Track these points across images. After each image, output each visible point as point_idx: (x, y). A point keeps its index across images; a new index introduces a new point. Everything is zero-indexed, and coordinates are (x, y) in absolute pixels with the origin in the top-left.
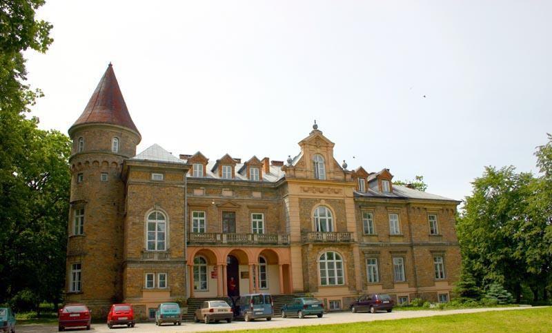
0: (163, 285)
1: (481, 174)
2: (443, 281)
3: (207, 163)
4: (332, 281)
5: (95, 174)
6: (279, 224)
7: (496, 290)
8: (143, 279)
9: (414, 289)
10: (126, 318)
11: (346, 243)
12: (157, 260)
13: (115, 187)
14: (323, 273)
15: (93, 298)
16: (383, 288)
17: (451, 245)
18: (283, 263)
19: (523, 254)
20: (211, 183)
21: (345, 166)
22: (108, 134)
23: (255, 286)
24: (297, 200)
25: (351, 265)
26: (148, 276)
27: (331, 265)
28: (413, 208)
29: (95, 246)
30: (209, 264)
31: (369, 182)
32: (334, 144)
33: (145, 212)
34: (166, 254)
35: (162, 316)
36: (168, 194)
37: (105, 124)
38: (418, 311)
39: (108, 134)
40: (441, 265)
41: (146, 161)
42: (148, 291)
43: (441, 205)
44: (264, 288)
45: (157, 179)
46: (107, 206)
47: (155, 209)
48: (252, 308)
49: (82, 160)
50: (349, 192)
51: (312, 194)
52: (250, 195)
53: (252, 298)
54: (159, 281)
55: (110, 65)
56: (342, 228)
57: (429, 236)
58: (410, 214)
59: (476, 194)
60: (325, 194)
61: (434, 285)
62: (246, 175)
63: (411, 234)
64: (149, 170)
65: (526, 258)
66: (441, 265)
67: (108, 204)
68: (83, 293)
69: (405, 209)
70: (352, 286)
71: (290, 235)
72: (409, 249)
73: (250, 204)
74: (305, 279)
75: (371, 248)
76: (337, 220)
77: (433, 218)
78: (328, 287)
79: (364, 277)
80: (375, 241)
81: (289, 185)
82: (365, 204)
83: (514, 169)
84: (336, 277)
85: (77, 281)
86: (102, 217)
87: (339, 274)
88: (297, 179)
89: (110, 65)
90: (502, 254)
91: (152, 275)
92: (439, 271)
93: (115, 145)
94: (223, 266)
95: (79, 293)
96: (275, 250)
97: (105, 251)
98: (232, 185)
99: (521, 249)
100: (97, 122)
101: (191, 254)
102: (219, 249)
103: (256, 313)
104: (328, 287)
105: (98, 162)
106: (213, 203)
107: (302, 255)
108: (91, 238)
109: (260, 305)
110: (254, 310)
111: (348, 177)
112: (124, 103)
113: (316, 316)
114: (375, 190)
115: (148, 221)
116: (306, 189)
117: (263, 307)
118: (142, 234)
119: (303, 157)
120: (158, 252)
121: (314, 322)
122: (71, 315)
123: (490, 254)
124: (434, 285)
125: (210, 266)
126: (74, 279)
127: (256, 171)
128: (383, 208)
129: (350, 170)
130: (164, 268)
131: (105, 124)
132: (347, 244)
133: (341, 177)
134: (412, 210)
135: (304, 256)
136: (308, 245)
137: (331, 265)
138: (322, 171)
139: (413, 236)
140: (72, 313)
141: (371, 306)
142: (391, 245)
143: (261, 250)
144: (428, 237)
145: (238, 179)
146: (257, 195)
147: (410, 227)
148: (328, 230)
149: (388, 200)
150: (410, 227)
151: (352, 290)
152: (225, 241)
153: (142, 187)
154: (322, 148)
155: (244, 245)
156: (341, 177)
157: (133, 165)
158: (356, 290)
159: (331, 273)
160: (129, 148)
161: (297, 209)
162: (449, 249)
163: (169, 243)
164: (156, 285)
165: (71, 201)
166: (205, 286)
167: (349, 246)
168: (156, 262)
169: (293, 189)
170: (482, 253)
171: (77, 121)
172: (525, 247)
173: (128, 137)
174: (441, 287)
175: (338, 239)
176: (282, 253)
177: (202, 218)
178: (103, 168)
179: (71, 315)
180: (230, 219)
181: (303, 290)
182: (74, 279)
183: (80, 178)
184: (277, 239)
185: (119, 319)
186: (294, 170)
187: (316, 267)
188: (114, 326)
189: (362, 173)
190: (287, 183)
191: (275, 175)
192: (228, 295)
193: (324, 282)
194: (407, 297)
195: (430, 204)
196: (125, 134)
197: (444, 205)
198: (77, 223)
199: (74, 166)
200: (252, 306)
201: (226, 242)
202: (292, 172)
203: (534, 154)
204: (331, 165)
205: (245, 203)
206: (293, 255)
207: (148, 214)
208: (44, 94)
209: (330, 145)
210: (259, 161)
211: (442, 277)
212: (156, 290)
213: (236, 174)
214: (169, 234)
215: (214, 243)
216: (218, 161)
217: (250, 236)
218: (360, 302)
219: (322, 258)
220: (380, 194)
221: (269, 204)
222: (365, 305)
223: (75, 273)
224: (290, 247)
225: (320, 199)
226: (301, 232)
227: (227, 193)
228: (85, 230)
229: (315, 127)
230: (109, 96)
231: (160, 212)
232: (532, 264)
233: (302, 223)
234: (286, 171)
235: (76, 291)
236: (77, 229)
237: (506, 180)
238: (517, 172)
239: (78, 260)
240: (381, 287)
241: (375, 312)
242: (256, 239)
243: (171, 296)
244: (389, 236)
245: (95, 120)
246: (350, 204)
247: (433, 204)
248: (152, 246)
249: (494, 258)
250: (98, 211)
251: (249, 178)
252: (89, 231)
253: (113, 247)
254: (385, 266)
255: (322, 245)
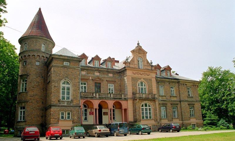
0: (69, 117)
1: (206, 70)
2: (193, 118)
3: (87, 59)
4: (147, 117)
5: (33, 61)
6: (121, 89)
7: (222, 122)
8: (59, 115)
9: (181, 122)
10: (58, 135)
11: (153, 99)
12: (66, 105)
13: (43, 68)
14: (143, 113)
15: (31, 124)
16: (168, 121)
17: (197, 101)
18: (124, 108)
19: (226, 107)
20: (90, 68)
21: (152, 63)
22: (40, 42)
23: (111, 119)
24: (131, 78)
25: (155, 110)
26: (62, 113)
27: (146, 110)
28: (181, 84)
29: (32, 98)
30: (88, 108)
31: (161, 71)
32: (147, 52)
33: (61, 81)
34: (71, 102)
35: (76, 134)
36: (72, 72)
37: (38, 37)
38: (193, 132)
39: (40, 42)
40: (192, 110)
41: (61, 55)
42: (62, 121)
43: (193, 83)
44: (86, 121)
45: (66, 65)
46: (39, 78)
47: (65, 80)
48: (119, 130)
49: (27, 54)
50: (154, 75)
51: (137, 76)
52: (108, 75)
53: (118, 124)
54: (67, 116)
55: (40, 9)
56: (151, 92)
57: (188, 97)
58: (180, 87)
59: (203, 79)
60: (143, 76)
61: (190, 120)
62: (105, 66)
63: (180, 96)
64: (62, 60)
65: (228, 108)
66: (192, 110)
67: (39, 77)
68: (26, 122)
69: (177, 84)
70: (156, 120)
71: (127, 95)
72: (179, 103)
73: (107, 79)
74: (135, 116)
75: (163, 102)
76: (148, 88)
77: (189, 89)
78: (145, 120)
79: (160, 116)
80: (164, 98)
81: (127, 71)
82: (160, 81)
83: (222, 68)
84: (149, 115)
85: (22, 115)
86: (37, 83)
87: (150, 113)
88: (131, 68)
89: (40, 9)
90: (217, 106)
91: (69, 113)
92: (192, 113)
93: (43, 48)
94: (96, 109)
95: (24, 122)
96: (120, 102)
97: (37, 100)
98: (99, 70)
99: (226, 104)
100: (35, 36)
101: (82, 102)
102: (95, 101)
103: (121, 132)
104: (145, 120)
105: (35, 56)
106: (90, 78)
107: (133, 105)
108: (30, 93)
109: (122, 128)
110: (120, 130)
111: (153, 68)
112: (47, 27)
113: (147, 134)
114: (164, 74)
115: (62, 85)
116: (135, 73)
117: (124, 129)
118: (59, 92)
119: (133, 58)
120: (67, 101)
121: (146, 137)
122: (30, 133)
123: (211, 107)
124: (190, 120)
125: (88, 109)
126: (21, 114)
127: (110, 63)
128: (168, 83)
129: (154, 65)
130: (69, 109)
131: (38, 37)
132: (153, 100)
133: (150, 68)
134: (180, 85)
135: (134, 105)
136: (136, 99)
137: (146, 110)
138: (141, 65)
139: (181, 97)
140: (31, 132)
141: (171, 129)
142: (171, 101)
143: (115, 101)
144: (187, 97)
145: (88, 66)
146: (111, 75)
147: (179, 92)
148: (144, 93)
149: (170, 80)
150: (179, 92)
151: (156, 121)
152: (97, 97)
153: (59, 68)
154: (142, 54)
155: (106, 99)
156: (150, 68)
157: (55, 57)
158: (157, 121)
159: (146, 113)
160: (50, 49)
161: (131, 83)
162: (196, 103)
163: (72, 97)
164: (65, 118)
165: (20, 75)
166: (86, 119)
167: (154, 100)
168: (66, 106)
169: (129, 73)
170: (207, 106)
171: (25, 34)
172: (228, 103)
173: (49, 44)
174: (193, 121)
175: (150, 97)
176: (124, 104)
177: (85, 86)
178: (37, 59)
179: (30, 133)
180: (98, 86)
181: (133, 121)
182: (21, 114)
183: (25, 64)
184: (122, 97)
185: (55, 135)
186: (129, 64)
187: (140, 110)
188: (76, 137)
189: (158, 67)
190: (126, 69)
191: (119, 66)
192: (99, 123)
193: (143, 118)
194: (195, 124)
195: (188, 83)
196: (48, 43)
197: (194, 83)
198: (23, 86)
199: (22, 57)
200: (119, 128)
201: (98, 97)
202: (128, 64)
203: (232, 61)
204: (146, 62)
205: (105, 79)
206: (129, 104)
207: (62, 81)
208: (7, 21)
209: (145, 53)
210: (111, 58)
211: (193, 116)
212: (65, 120)
213: (88, 64)
214: (72, 92)
215: (92, 98)
216: (92, 58)
217: (109, 95)
218: (164, 127)
219: (143, 106)
220: (166, 77)
221: (116, 80)
222: (166, 129)
223: (22, 111)
224: (127, 101)
225: (141, 78)
226: (133, 93)
227: (97, 74)
228: (27, 89)
229: (138, 44)
230: (39, 23)
231: (68, 81)
232: (231, 111)
233: (133, 89)
234: (125, 64)
235: (22, 120)
236: (23, 89)
237: (218, 73)
238: (223, 70)
239: (23, 105)
240: (178, 120)
241: (172, 132)
242: (112, 96)
243: (73, 123)
244: (171, 96)
245: (33, 34)
246: (154, 80)
247: (190, 83)
248: (63, 98)
249: (213, 108)
250: (34, 79)
251: (107, 67)
252: (29, 89)
253: (41, 98)
254: (169, 110)
255: (142, 100)
